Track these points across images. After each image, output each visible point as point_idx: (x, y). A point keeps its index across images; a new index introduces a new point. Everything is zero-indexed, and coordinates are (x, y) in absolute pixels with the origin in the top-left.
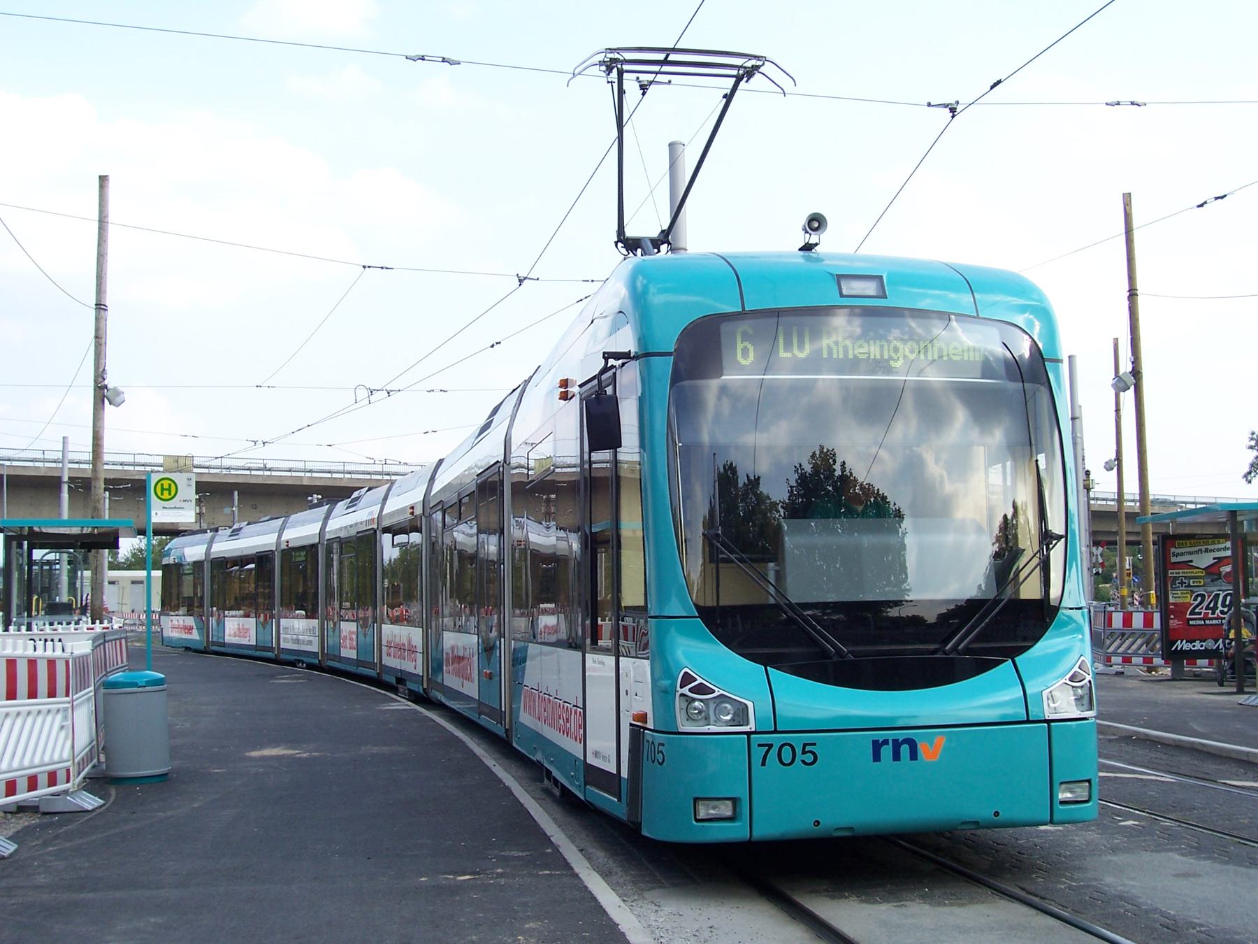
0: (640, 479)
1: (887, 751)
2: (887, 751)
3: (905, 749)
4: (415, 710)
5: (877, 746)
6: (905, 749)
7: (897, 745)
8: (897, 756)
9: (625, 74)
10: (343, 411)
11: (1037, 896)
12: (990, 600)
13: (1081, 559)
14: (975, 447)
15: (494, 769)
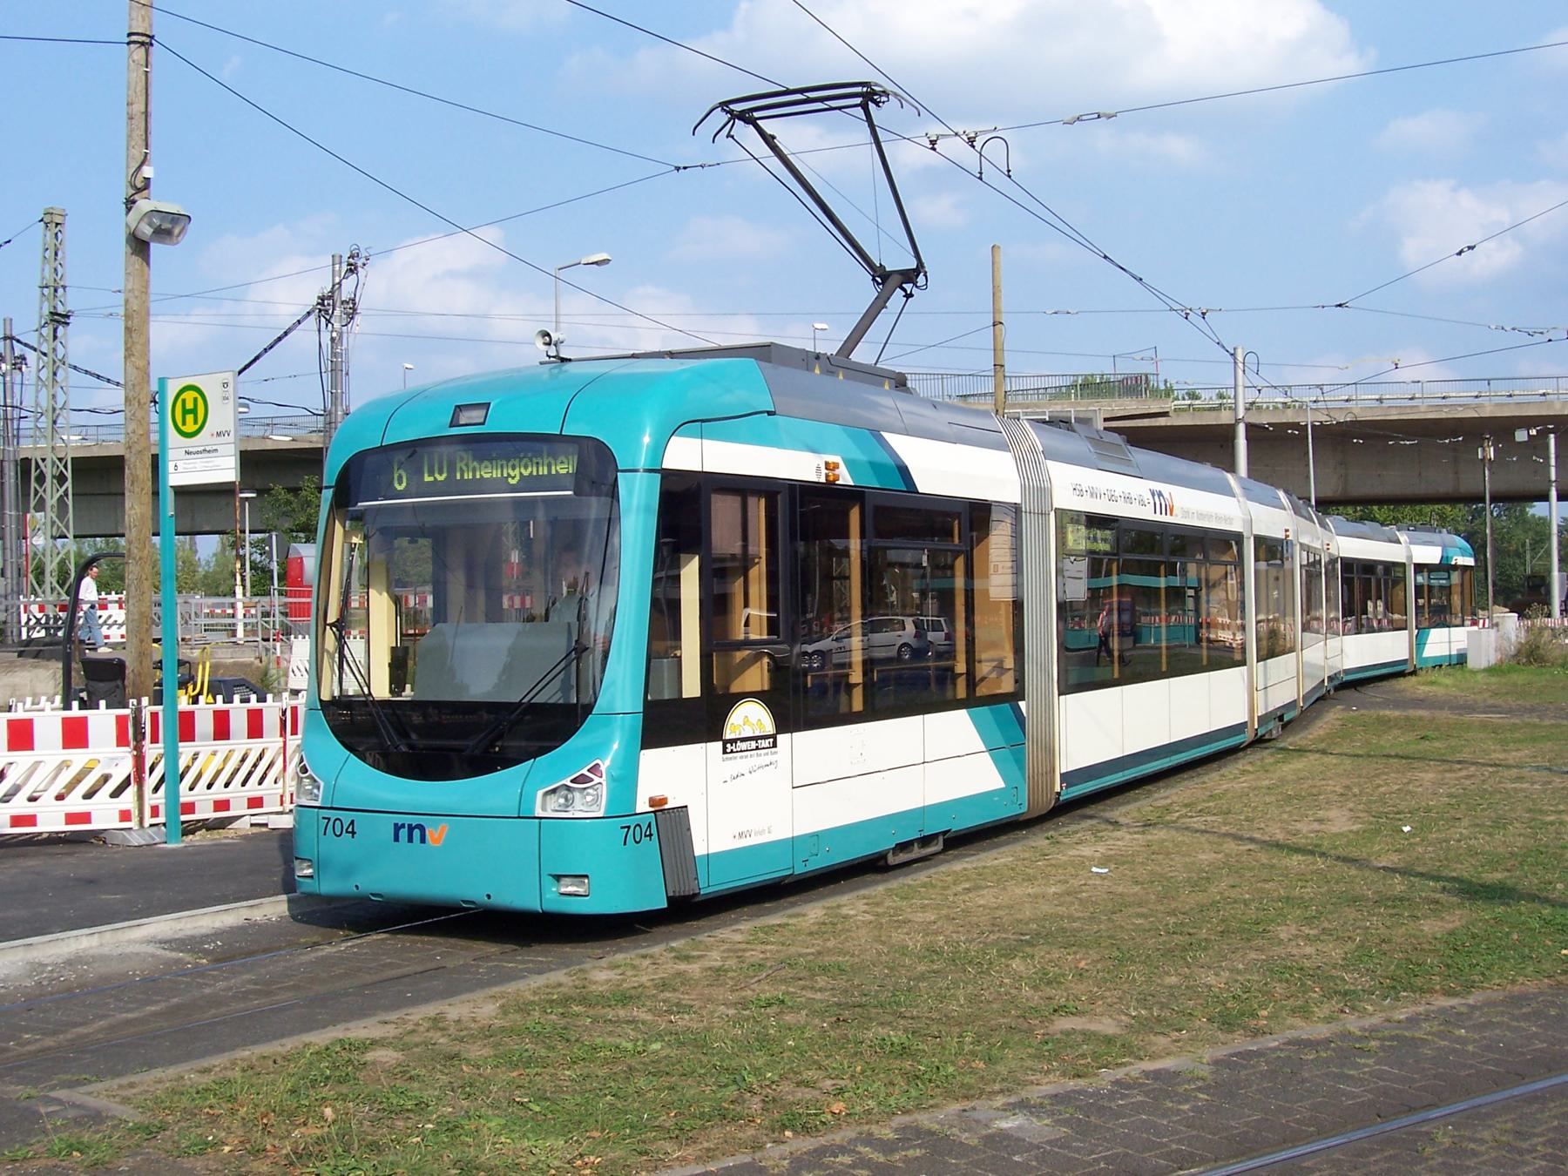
0: (1018, 606)
1: (404, 833)
2: (404, 833)
3: (417, 833)
4: (67, 505)
5: (397, 828)
6: (417, 833)
7: (411, 828)
8: (410, 840)
9: (738, 499)
10: (1161, 296)
11: (1248, 839)
12: (129, 776)
13: (255, 766)
14: (766, 688)
15: (1121, 774)
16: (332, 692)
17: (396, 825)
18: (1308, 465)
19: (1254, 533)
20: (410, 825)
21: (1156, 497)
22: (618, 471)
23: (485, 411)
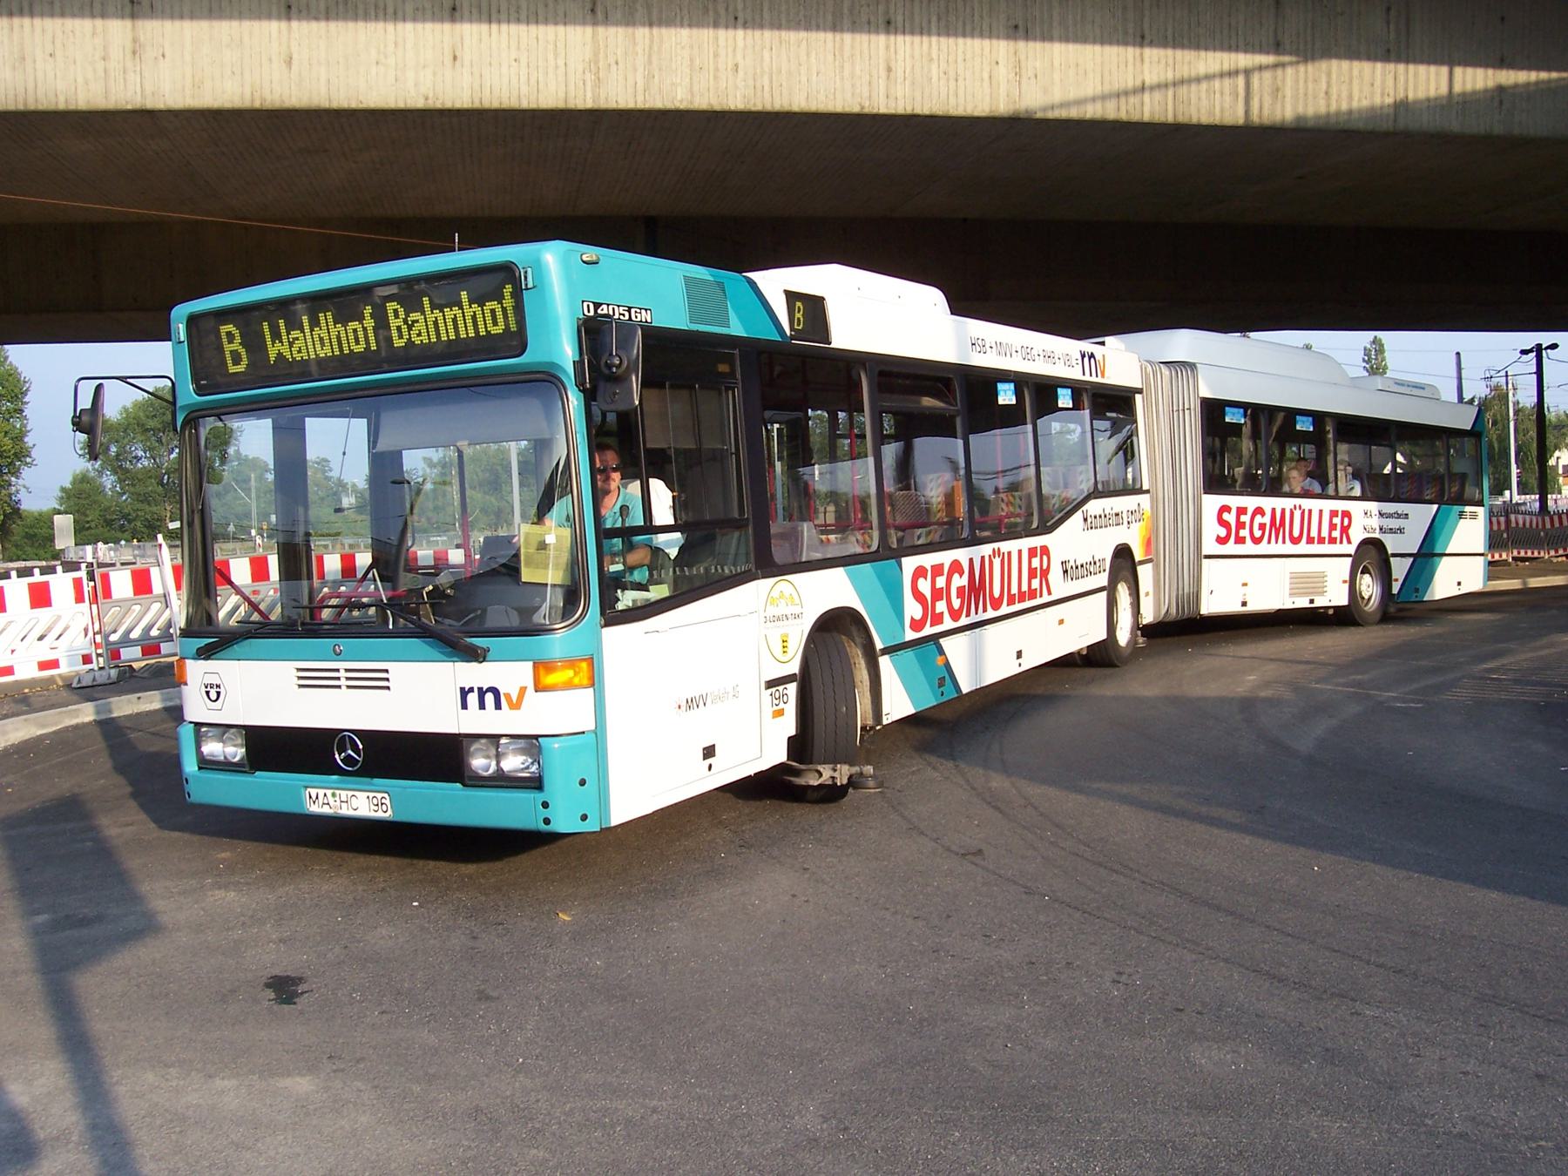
1: (473, 699)
2: (473, 699)
3: (489, 698)
5: (464, 693)
6: (489, 698)
8: (482, 706)
16: (1428, 90)
17: (462, 689)
18: (308, 227)
19: (1201, 395)
20: (480, 689)
21: (1086, 359)
22: (699, 450)
23: (1071, 406)
